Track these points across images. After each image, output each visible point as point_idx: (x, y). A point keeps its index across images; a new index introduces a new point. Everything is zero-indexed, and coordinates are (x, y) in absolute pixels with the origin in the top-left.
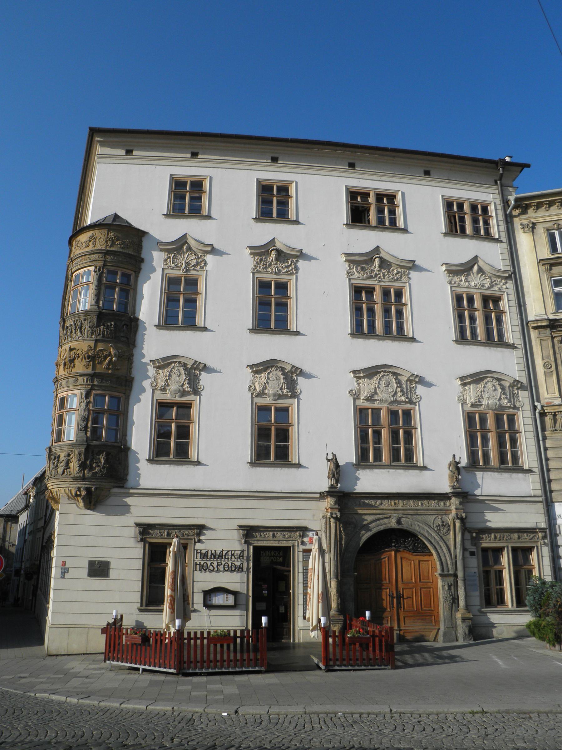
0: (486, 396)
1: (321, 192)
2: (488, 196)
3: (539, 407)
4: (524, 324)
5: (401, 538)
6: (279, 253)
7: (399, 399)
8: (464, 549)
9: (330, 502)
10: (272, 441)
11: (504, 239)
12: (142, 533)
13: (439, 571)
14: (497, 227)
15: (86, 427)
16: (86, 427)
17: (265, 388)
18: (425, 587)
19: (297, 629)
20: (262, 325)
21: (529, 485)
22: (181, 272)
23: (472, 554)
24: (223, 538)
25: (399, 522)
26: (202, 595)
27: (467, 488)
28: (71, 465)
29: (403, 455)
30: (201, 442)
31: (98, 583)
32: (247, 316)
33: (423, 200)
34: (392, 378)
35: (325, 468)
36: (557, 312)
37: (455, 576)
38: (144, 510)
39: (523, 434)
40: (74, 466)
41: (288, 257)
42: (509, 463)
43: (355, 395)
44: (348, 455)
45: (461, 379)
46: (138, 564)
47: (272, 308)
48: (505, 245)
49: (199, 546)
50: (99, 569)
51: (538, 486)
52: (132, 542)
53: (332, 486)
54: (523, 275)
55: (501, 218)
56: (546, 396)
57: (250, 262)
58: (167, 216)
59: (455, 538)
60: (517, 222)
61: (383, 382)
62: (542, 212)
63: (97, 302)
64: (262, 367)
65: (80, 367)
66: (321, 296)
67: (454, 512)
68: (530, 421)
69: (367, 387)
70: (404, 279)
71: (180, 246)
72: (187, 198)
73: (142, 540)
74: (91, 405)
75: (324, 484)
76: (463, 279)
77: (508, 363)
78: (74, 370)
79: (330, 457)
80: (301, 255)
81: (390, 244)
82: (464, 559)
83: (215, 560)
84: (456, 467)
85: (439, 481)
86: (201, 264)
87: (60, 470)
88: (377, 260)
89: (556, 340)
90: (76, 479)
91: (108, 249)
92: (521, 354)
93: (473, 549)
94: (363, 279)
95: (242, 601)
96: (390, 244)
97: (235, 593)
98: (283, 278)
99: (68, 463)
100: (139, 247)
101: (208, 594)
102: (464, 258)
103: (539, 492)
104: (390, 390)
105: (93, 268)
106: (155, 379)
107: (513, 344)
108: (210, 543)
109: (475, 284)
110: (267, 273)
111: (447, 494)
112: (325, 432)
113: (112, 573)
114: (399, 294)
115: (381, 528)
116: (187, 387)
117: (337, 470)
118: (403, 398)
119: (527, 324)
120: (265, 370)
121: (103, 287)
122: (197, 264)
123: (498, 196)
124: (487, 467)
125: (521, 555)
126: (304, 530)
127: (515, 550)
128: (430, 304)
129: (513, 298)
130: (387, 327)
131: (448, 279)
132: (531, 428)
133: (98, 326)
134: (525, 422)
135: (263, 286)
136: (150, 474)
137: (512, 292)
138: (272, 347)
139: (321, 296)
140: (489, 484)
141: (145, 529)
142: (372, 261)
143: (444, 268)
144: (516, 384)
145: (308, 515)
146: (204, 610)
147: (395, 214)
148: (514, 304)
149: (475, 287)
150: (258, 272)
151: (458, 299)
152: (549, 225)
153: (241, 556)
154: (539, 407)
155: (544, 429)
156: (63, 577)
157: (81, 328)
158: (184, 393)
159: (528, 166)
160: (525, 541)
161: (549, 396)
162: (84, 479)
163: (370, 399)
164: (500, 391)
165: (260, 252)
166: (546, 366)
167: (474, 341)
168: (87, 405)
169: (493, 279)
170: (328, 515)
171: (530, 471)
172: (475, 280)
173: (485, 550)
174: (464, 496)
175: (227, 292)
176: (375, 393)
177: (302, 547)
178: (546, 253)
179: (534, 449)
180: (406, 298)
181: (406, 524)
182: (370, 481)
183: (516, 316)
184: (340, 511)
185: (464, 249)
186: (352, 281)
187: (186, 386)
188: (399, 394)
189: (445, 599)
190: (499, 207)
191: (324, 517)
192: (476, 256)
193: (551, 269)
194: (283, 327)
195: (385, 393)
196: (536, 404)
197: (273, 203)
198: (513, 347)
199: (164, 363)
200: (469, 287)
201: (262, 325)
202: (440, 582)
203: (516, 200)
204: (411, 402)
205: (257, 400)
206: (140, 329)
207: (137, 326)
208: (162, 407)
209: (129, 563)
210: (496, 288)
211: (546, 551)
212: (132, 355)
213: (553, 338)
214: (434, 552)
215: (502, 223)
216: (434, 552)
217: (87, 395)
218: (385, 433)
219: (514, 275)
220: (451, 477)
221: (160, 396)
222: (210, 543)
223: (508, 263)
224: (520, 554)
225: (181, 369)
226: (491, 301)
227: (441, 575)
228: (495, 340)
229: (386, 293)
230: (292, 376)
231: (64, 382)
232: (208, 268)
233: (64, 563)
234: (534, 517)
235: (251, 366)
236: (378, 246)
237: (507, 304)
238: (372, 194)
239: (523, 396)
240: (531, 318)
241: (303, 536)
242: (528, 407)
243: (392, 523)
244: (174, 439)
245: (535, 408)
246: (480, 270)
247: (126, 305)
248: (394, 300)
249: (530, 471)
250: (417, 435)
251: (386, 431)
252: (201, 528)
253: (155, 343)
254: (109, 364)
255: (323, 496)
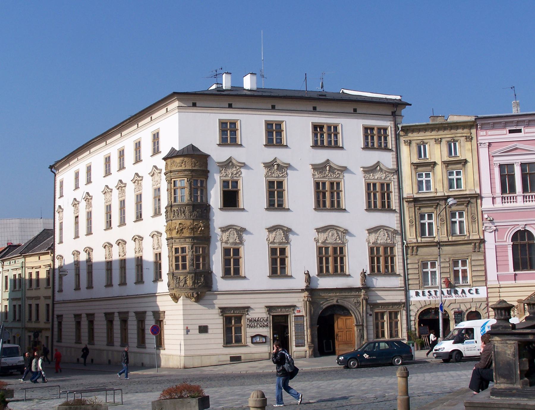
0: (380, 238)
1: (298, 126)
2: (388, 124)
3: (405, 244)
4: (401, 199)
5: (341, 310)
6: (278, 165)
7: (338, 242)
8: (367, 313)
9: (306, 294)
10: (278, 263)
11: (394, 149)
12: (221, 312)
13: (355, 323)
14: (391, 143)
15: (193, 263)
16: (193, 263)
17: (274, 239)
18: (349, 330)
19: (293, 351)
20: (270, 143)
21: (398, 282)
22: (229, 178)
23: (371, 315)
24: (259, 312)
25: (337, 301)
26: (250, 339)
27: (369, 285)
28: (188, 282)
29: (339, 270)
30: (245, 267)
31: (203, 335)
32: (264, 203)
33: (351, 129)
34: (335, 232)
35: (304, 277)
36: (418, 193)
37: (363, 325)
38: (223, 301)
39: (397, 257)
40: (189, 282)
41: (284, 168)
42: (390, 272)
43: (317, 241)
44: (314, 272)
45: (368, 230)
46: (221, 326)
47: (276, 197)
48: (394, 153)
49: (247, 316)
50: (203, 329)
51: (403, 282)
52: (217, 316)
53: (307, 286)
54: (402, 171)
55: (393, 136)
56: (409, 237)
57: (264, 171)
58: (219, 145)
59: (362, 308)
60: (402, 139)
61: (330, 234)
62: (415, 134)
63: (191, 198)
64: (272, 229)
65: (186, 233)
66: (300, 189)
67: (363, 296)
68: (400, 250)
69: (322, 237)
70: (341, 177)
71: (228, 164)
72: (229, 134)
73: (222, 315)
74: (194, 253)
75: (303, 285)
76: (371, 175)
77: (390, 220)
78: (183, 235)
79: (306, 272)
80: (289, 166)
81: (335, 157)
82: (367, 317)
83: (254, 323)
84: (364, 274)
85: (356, 282)
86: (239, 173)
87: (182, 284)
88: (328, 167)
89: (416, 208)
90: (191, 289)
91: (193, 168)
92: (398, 215)
93: (371, 313)
94: (320, 178)
95: (268, 340)
96: (335, 157)
97: (265, 337)
98: (281, 179)
99: (185, 281)
100: (206, 164)
101: (252, 337)
102: (371, 163)
103: (403, 285)
104: (334, 238)
105: (186, 179)
106: (222, 237)
107: (395, 210)
108: (252, 315)
109: (378, 177)
110: (272, 177)
111: (359, 288)
112: (303, 260)
113: (210, 331)
114: (338, 184)
115: (329, 304)
116: (237, 241)
117: (309, 278)
118: (340, 241)
119: (403, 199)
120: (275, 230)
121: (192, 190)
122: (237, 173)
123: (392, 123)
124: (379, 273)
125: (393, 316)
126: (294, 307)
127: (390, 313)
128: (353, 191)
129: (396, 184)
130: (332, 203)
131: (364, 175)
132: (401, 254)
133: (193, 211)
134: (398, 251)
135: (270, 184)
136: (221, 284)
137: (396, 180)
138: (277, 218)
139: (300, 189)
140: (379, 282)
141: (223, 310)
142: (326, 167)
143: (362, 169)
144: (395, 232)
145: (296, 300)
146: (252, 345)
147: (285, 264)
148: (396, 187)
149: (377, 179)
150: (268, 176)
151: (368, 185)
152: (418, 142)
153: (267, 320)
154: (405, 244)
155: (407, 254)
156: (187, 334)
157: (184, 212)
158: (236, 244)
159: (411, 105)
160: (395, 309)
161: (411, 237)
162: (194, 289)
163: (323, 243)
164: (387, 235)
165: (318, 168)
166: (410, 222)
167: (375, 209)
168: (193, 252)
169: (387, 174)
170: (306, 299)
171: (399, 275)
172: (378, 175)
173: (377, 314)
174: (366, 288)
175: (253, 190)
176: (326, 239)
177: (293, 315)
178: (416, 160)
179: (402, 264)
180: (342, 187)
181: (340, 302)
182: (325, 283)
183: (397, 194)
184: (311, 297)
185: (373, 157)
186: (315, 179)
187: (237, 240)
188: (338, 239)
189: (358, 337)
190: (393, 129)
191: (304, 300)
192: (379, 162)
193: (417, 168)
194: (281, 207)
195: (331, 238)
196: (404, 241)
197: (274, 135)
198: (394, 211)
199: (224, 229)
200: (374, 179)
201: (270, 143)
202: (355, 328)
203: (402, 127)
204: (343, 243)
205: (270, 245)
206: (211, 210)
207: (210, 209)
208: (226, 251)
209: (216, 325)
210: (388, 179)
211: (404, 313)
212: (209, 225)
213: (415, 207)
214: (353, 315)
215: (394, 139)
216: (353, 315)
217: (192, 248)
218: (331, 259)
219: (398, 171)
220: (362, 280)
221: (224, 245)
222: (252, 315)
223: (395, 163)
224: (140, 280)
225: (235, 231)
226: (385, 188)
227: (356, 325)
228: (386, 207)
229: (332, 184)
230: (287, 231)
231: (177, 240)
232: (242, 175)
233: (187, 328)
234: (399, 297)
235: (267, 229)
236: (328, 160)
237: (393, 188)
238: (325, 126)
239: (398, 238)
240: (405, 196)
241: (293, 310)
242: (400, 243)
243: (334, 302)
244: (233, 267)
245: (403, 243)
246: (381, 170)
247: (204, 199)
248: (336, 188)
249: (399, 275)
250: (346, 260)
251: (331, 258)
252: (248, 308)
253: (220, 218)
254: (200, 231)
255: (303, 291)
